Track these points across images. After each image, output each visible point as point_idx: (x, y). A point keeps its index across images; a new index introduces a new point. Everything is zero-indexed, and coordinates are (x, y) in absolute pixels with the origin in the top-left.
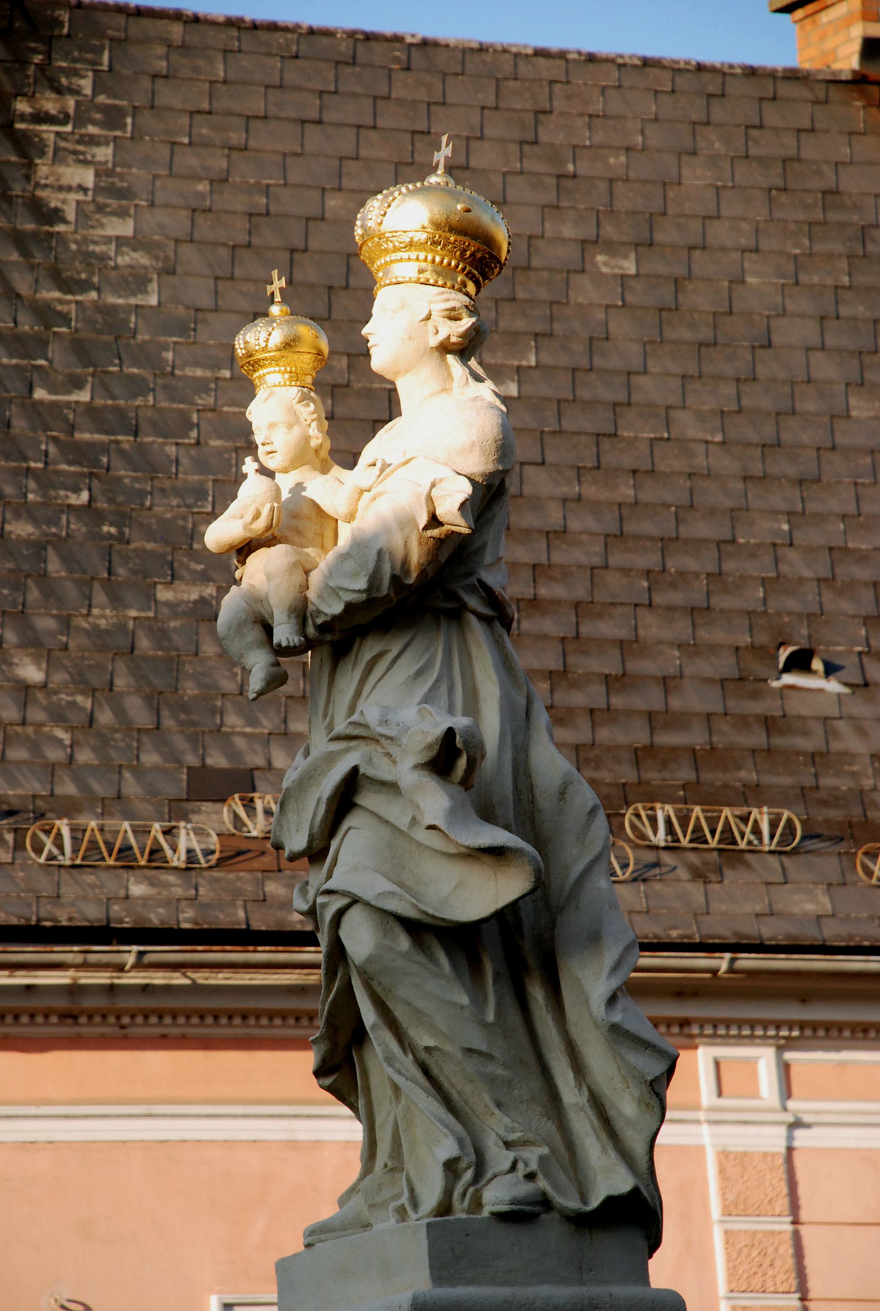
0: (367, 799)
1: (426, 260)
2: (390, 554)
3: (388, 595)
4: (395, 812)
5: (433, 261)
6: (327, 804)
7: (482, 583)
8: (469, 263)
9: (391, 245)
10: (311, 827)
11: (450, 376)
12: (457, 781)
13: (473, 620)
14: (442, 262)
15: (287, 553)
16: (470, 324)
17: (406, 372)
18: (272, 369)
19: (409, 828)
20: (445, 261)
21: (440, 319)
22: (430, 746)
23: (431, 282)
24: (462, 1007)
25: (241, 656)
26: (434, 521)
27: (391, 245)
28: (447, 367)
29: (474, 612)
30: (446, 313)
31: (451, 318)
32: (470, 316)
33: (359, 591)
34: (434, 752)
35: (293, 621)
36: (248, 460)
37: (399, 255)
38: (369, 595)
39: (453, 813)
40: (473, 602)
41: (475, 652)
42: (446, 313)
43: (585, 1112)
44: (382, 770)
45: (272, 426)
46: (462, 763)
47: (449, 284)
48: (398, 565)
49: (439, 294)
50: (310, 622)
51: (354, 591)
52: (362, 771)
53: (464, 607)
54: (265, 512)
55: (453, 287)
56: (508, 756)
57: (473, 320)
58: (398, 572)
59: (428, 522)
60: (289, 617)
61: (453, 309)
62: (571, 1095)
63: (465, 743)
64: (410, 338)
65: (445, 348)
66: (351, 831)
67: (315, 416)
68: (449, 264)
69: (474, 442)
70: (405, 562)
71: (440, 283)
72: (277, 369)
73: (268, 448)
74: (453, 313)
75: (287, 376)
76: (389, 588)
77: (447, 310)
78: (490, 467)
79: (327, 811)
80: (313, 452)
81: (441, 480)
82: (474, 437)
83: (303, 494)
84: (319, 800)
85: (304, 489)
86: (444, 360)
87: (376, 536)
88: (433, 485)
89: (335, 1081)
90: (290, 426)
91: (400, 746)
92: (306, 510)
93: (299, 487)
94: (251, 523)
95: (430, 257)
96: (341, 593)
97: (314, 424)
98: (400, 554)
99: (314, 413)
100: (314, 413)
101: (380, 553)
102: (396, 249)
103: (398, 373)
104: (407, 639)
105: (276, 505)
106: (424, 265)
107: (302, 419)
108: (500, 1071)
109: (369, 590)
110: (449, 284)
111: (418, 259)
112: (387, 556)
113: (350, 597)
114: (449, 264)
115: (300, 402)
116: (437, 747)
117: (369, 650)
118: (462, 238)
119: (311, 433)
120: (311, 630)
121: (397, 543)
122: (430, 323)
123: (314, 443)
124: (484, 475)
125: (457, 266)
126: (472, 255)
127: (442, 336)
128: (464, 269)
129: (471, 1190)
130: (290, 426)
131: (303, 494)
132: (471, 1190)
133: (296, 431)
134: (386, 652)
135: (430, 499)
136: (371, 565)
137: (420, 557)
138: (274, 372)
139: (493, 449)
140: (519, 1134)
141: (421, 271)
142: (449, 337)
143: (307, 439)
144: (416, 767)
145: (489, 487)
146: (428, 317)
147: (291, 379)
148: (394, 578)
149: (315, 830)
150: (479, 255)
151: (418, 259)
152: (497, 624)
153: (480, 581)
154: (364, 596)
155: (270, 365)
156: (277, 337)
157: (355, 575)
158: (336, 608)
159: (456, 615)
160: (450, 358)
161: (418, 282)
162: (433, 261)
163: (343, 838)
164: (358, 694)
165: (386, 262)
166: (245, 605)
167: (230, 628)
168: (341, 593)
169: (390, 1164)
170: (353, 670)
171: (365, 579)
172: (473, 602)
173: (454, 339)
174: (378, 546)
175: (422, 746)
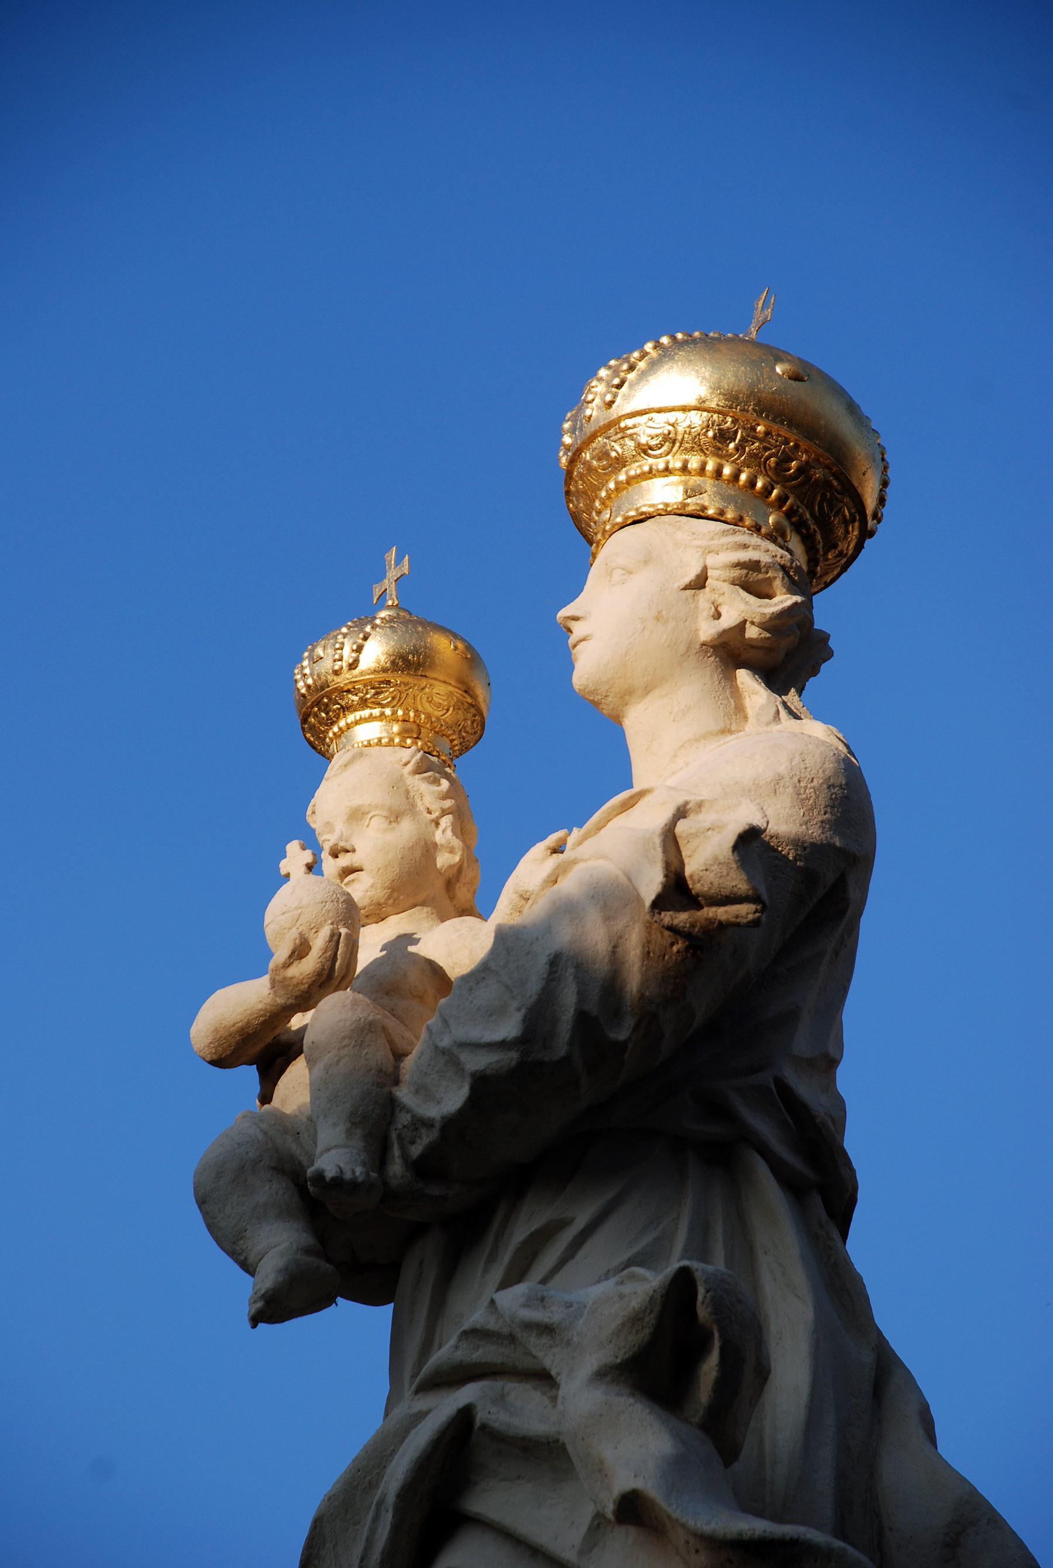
2: (578, 966)
3: (566, 1059)
6: (397, 1509)
7: (785, 1091)
8: (793, 489)
9: (630, 444)
11: (740, 710)
12: (696, 1419)
13: (762, 1170)
14: (736, 477)
15: (355, 1003)
17: (647, 690)
20: (743, 477)
21: (726, 587)
22: (635, 1319)
23: (711, 512)
26: (677, 890)
27: (630, 444)
28: (736, 693)
30: (737, 573)
32: (791, 592)
33: (503, 1045)
35: (358, 1142)
36: (293, 847)
39: (677, 1469)
41: (761, 1238)
42: (737, 573)
44: (523, 1411)
45: (356, 815)
46: (710, 1367)
47: (748, 522)
49: (724, 533)
50: (396, 1152)
51: (491, 1046)
54: (319, 942)
55: (756, 529)
56: (826, 1454)
57: (798, 599)
58: (592, 1007)
59: (665, 887)
60: (349, 1133)
61: (753, 566)
63: (717, 1306)
64: (658, 618)
65: (730, 652)
67: (448, 803)
69: (779, 778)
71: (730, 515)
72: (376, 712)
73: (344, 861)
74: (755, 576)
75: (396, 728)
76: (571, 1043)
78: (815, 833)
79: (396, 1528)
81: (700, 805)
82: (783, 769)
85: (416, 941)
86: (731, 679)
87: (546, 927)
88: (681, 813)
90: (395, 817)
91: (568, 1343)
92: (414, 977)
94: (287, 965)
95: (710, 466)
97: (446, 821)
98: (602, 966)
99: (445, 797)
100: (445, 797)
101: (555, 962)
102: (645, 450)
103: (628, 695)
104: (610, 1194)
105: (343, 931)
106: (695, 480)
107: (421, 807)
109: (523, 1041)
111: (684, 469)
113: (477, 1062)
114: (752, 483)
115: (419, 770)
116: (651, 1319)
120: (396, 1168)
121: (594, 936)
122: (704, 598)
123: (444, 860)
124: (797, 843)
125: (767, 491)
127: (729, 618)
128: (782, 500)
130: (395, 817)
133: (407, 829)
134: (561, 1225)
136: (534, 987)
137: (645, 982)
138: (371, 718)
139: (822, 801)
141: (691, 492)
142: (741, 627)
143: (429, 850)
144: (602, 1374)
145: (809, 877)
146: (700, 583)
147: (404, 733)
150: (818, 474)
151: (684, 469)
152: (817, 1200)
156: (376, 652)
157: (494, 1013)
158: (453, 1098)
159: (722, 1157)
160: (744, 677)
161: (682, 512)
162: (718, 473)
165: (618, 489)
166: (260, 1136)
167: (219, 1175)
170: (486, 1271)
173: (752, 632)
174: (553, 947)
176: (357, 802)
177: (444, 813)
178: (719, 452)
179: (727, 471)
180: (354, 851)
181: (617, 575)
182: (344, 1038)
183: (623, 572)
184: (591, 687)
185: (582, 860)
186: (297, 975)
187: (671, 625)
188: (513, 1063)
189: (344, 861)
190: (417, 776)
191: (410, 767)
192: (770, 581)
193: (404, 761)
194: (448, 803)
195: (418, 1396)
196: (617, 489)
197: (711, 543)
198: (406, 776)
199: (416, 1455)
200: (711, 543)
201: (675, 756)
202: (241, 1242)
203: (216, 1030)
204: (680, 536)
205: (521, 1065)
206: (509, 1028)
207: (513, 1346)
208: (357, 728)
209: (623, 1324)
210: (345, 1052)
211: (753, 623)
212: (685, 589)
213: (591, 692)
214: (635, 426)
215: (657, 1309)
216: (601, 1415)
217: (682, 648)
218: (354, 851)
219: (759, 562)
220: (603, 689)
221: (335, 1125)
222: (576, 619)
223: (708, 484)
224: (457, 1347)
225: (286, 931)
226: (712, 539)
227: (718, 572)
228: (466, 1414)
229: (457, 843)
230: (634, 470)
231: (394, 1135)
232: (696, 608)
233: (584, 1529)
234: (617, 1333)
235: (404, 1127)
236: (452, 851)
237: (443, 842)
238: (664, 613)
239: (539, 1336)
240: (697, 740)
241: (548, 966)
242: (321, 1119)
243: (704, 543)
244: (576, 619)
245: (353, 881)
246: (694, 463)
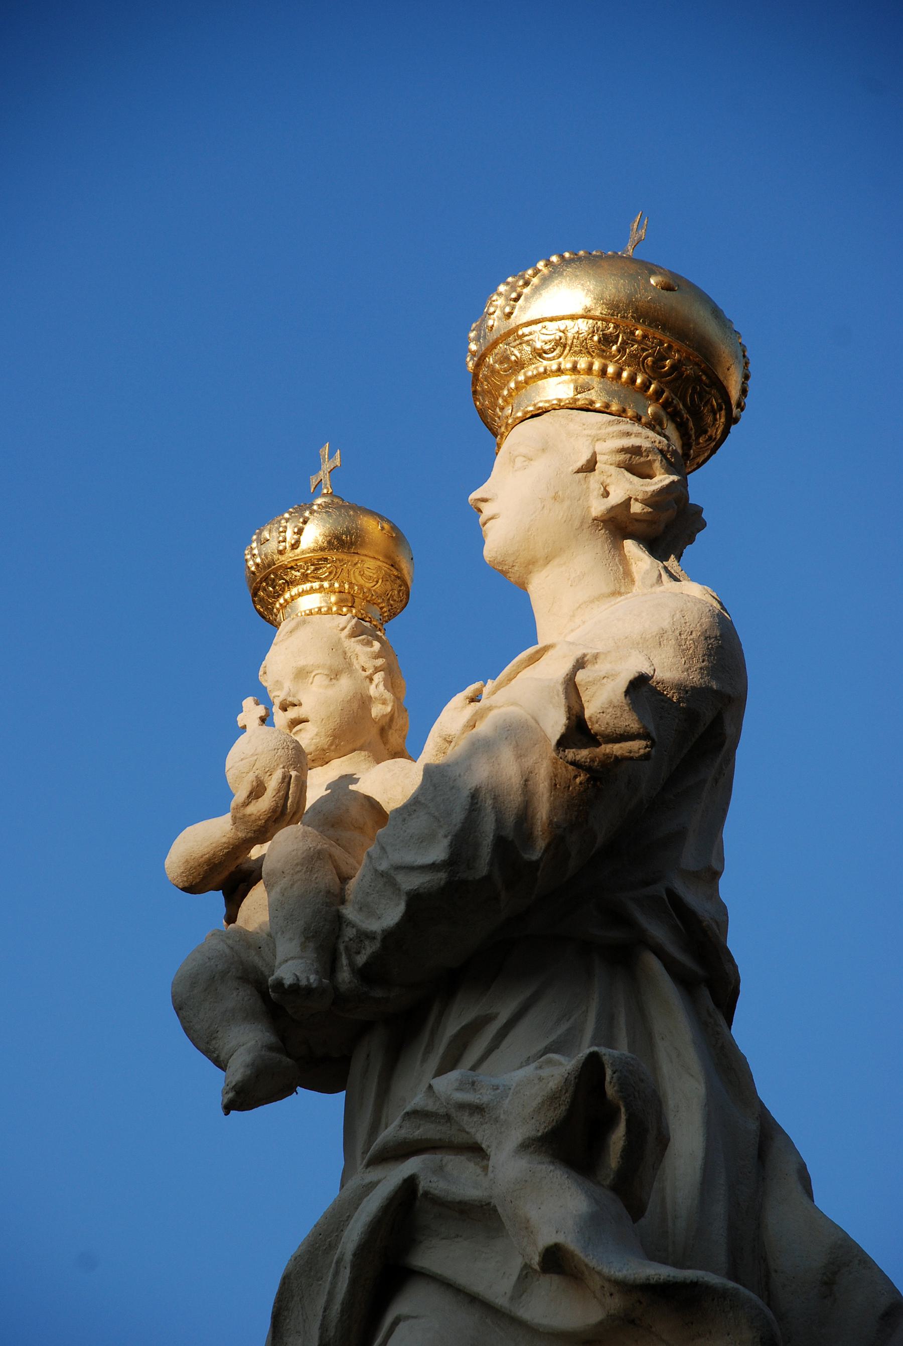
0: (436, 1256)
1: (589, 370)
3: (488, 878)
4: (491, 1272)
5: (603, 372)
6: (354, 1266)
8: (668, 384)
9: (528, 349)
10: (324, 1328)
11: (627, 574)
12: (607, 1182)
13: (654, 964)
14: (618, 375)
15: (305, 835)
16: (667, 482)
17: (548, 560)
19: (512, 1299)
20: (625, 375)
21: (613, 470)
22: (553, 1098)
23: (598, 405)
26: (578, 731)
27: (528, 349)
28: (624, 561)
29: (659, 952)
30: (622, 457)
31: (631, 469)
32: (669, 472)
33: (433, 867)
36: (248, 703)
37: (541, 365)
39: (593, 1224)
40: (658, 932)
42: (622, 457)
44: (460, 1180)
45: (302, 674)
46: (618, 1137)
47: (630, 413)
48: (510, 819)
50: (344, 961)
52: (423, 1185)
53: (644, 942)
54: (273, 784)
55: (637, 419)
58: (509, 832)
59: (568, 728)
60: (303, 946)
61: (636, 451)
63: (622, 1085)
64: (555, 498)
65: (618, 525)
66: (402, 1325)
67: (380, 662)
68: (632, 380)
69: (663, 633)
70: (525, 815)
71: (614, 408)
72: (316, 585)
73: (292, 713)
74: (637, 460)
75: (333, 598)
76: (491, 864)
77: (623, 450)
78: (695, 678)
79: (353, 1282)
80: (374, 731)
81: (596, 657)
82: (666, 624)
83: (352, 787)
85: (356, 781)
88: (580, 664)
90: (334, 675)
93: (349, 778)
94: (246, 804)
95: (596, 366)
96: (400, 878)
97: (379, 677)
98: (514, 800)
99: (377, 656)
100: (377, 656)
102: (540, 354)
103: (531, 565)
105: (293, 773)
107: (357, 666)
109: (450, 864)
110: (630, 413)
111: (574, 369)
112: (489, 802)
113: (411, 882)
114: (632, 380)
115: (353, 634)
116: (566, 1098)
118: (659, 335)
119: (373, 691)
120: (345, 975)
122: (594, 479)
123: (378, 711)
125: (646, 386)
126: (673, 367)
127: (616, 497)
128: (658, 394)
130: (334, 675)
131: (352, 787)
133: (345, 684)
135: (571, 687)
136: (458, 817)
137: (553, 810)
138: (312, 591)
139: (700, 651)
142: (627, 503)
143: (365, 702)
144: (525, 1146)
145: (691, 716)
146: (590, 466)
147: (340, 603)
148: (501, 842)
149: (332, 1332)
150: (689, 370)
151: (574, 369)
152: (705, 993)
153: (671, 893)
154: (442, 876)
157: (425, 840)
160: (630, 546)
161: (573, 406)
162: (603, 372)
170: (424, 1060)
172: (658, 932)
173: (636, 508)
175: (539, 1100)
176: (302, 662)
177: (377, 670)
180: (300, 705)
182: (297, 864)
183: (524, 459)
184: (500, 558)
186: (255, 812)
187: (567, 503)
188: (442, 883)
189: (292, 713)
190: (353, 639)
191: (346, 632)
192: (650, 463)
193: (341, 626)
194: (380, 662)
195: (368, 1170)
196: (517, 388)
197: (599, 432)
198: (343, 639)
199: (369, 1219)
200: (599, 432)
201: (573, 616)
202: (214, 1042)
203: (187, 861)
204: (572, 426)
206: (438, 853)
207: (449, 1124)
208: (300, 599)
211: (636, 500)
212: (578, 472)
213: (500, 563)
214: (531, 334)
216: (526, 1181)
217: (577, 523)
218: (300, 705)
219: (640, 447)
220: (510, 560)
221: (291, 939)
222: (485, 500)
223: (595, 381)
225: (244, 775)
226: (600, 428)
228: (410, 1183)
229: (388, 695)
230: (531, 371)
231: (342, 947)
232: (588, 488)
233: (514, 1278)
234: (538, 1110)
235: (351, 940)
236: (384, 703)
237: (377, 695)
238: (560, 493)
240: (592, 601)
241: (469, 799)
243: (593, 432)
245: (300, 730)
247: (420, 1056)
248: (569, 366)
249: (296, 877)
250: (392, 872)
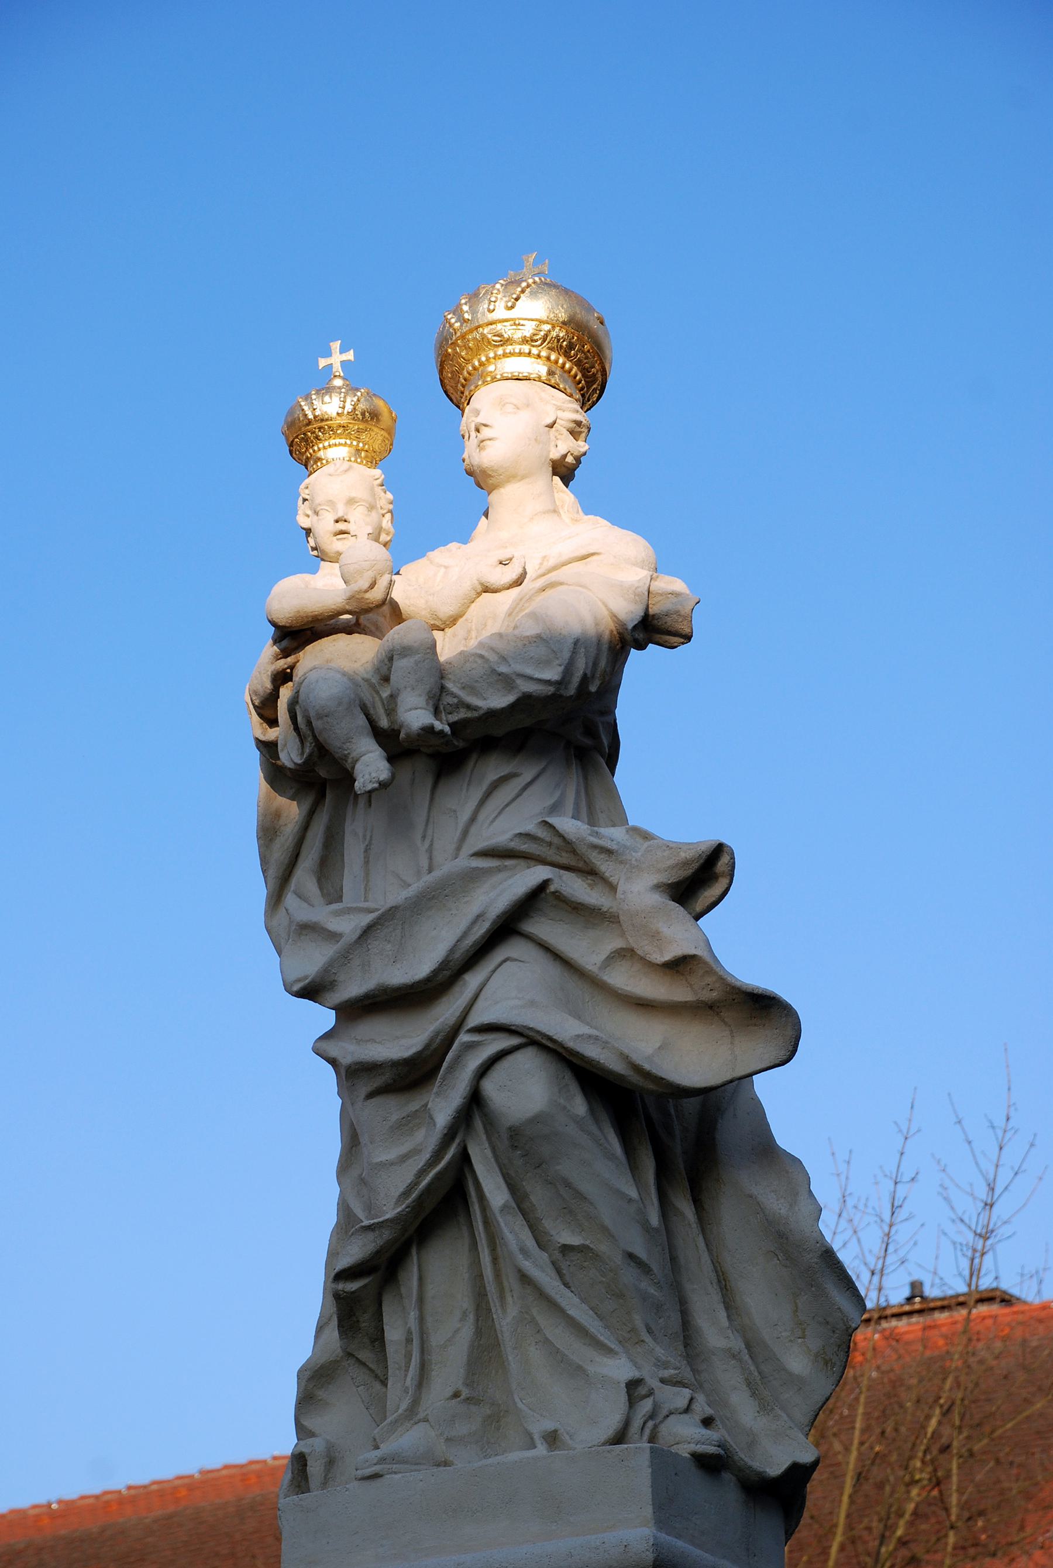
10: (452, 951)
17: (523, 478)
18: (343, 441)
19: (600, 968)
24: (630, 1200)
25: (348, 740)
30: (573, 425)
31: (572, 432)
33: (548, 682)
34: (689, 872)
38: (558, 689)
43: (740, 1361)
51: (540, 681)
61: (579, 423)
62: (714, 1332)
66: (508, 963)
67: (391, 507)
73: (342, 526)
84: (479, 917)
89: (365, 1286)
95: (561, 361)
96: (519, 681)
97: (388, 516)
103: (512, 477)
108: (652, 1290)
109: (559, 684)
116: (696, 866)
117: (493, 768)
127: (562, 449)
129: (650, 1424)
132: (650, 1424)
140: (672, 1372)
141: (551, 373)
142: (565, 456)
144: (658, 887)
146: (551, 426)
149: (457, 955)
151: (548, 358)
154: (551, 690)
155: (339, 436)
157: (545, 663)
162: (563, 367)
163: (494, 971)
164: (473, 819)
167: (340, 704)
168: (519, 681)
169: (465, 1393)
171: (561, 669)
176: (353, 495)
177: (390, 511)
178: (567, 355)
179: (567, 366)
181: (510, 408)
185: (561, 584)
189: (342, 526)
191: (379, 481)
194: (391, 507)
196: (494, 358)
199: (515, 898)
204: (543, 394)
205: (553, 695)
206: (553, 674)
209: (677, 865)
210: (427, 656)
215: (702, 861)
221: (420, 695)
222: (485, 425)
223: (558, 372)
224: (511, 840)
227: (562, 422)
229: (392, 530)
230: (509, 349)
231: (442, 707)
233: (604, 957)
234: (673, 867)
239: (600, 853)
242: (409, 689)
243: (559, 404)
244: (485, 425)
246: (553, 357)
247: (465, 785)
248: (527, 351)
249: (427, 656)
250: (514, 677)
